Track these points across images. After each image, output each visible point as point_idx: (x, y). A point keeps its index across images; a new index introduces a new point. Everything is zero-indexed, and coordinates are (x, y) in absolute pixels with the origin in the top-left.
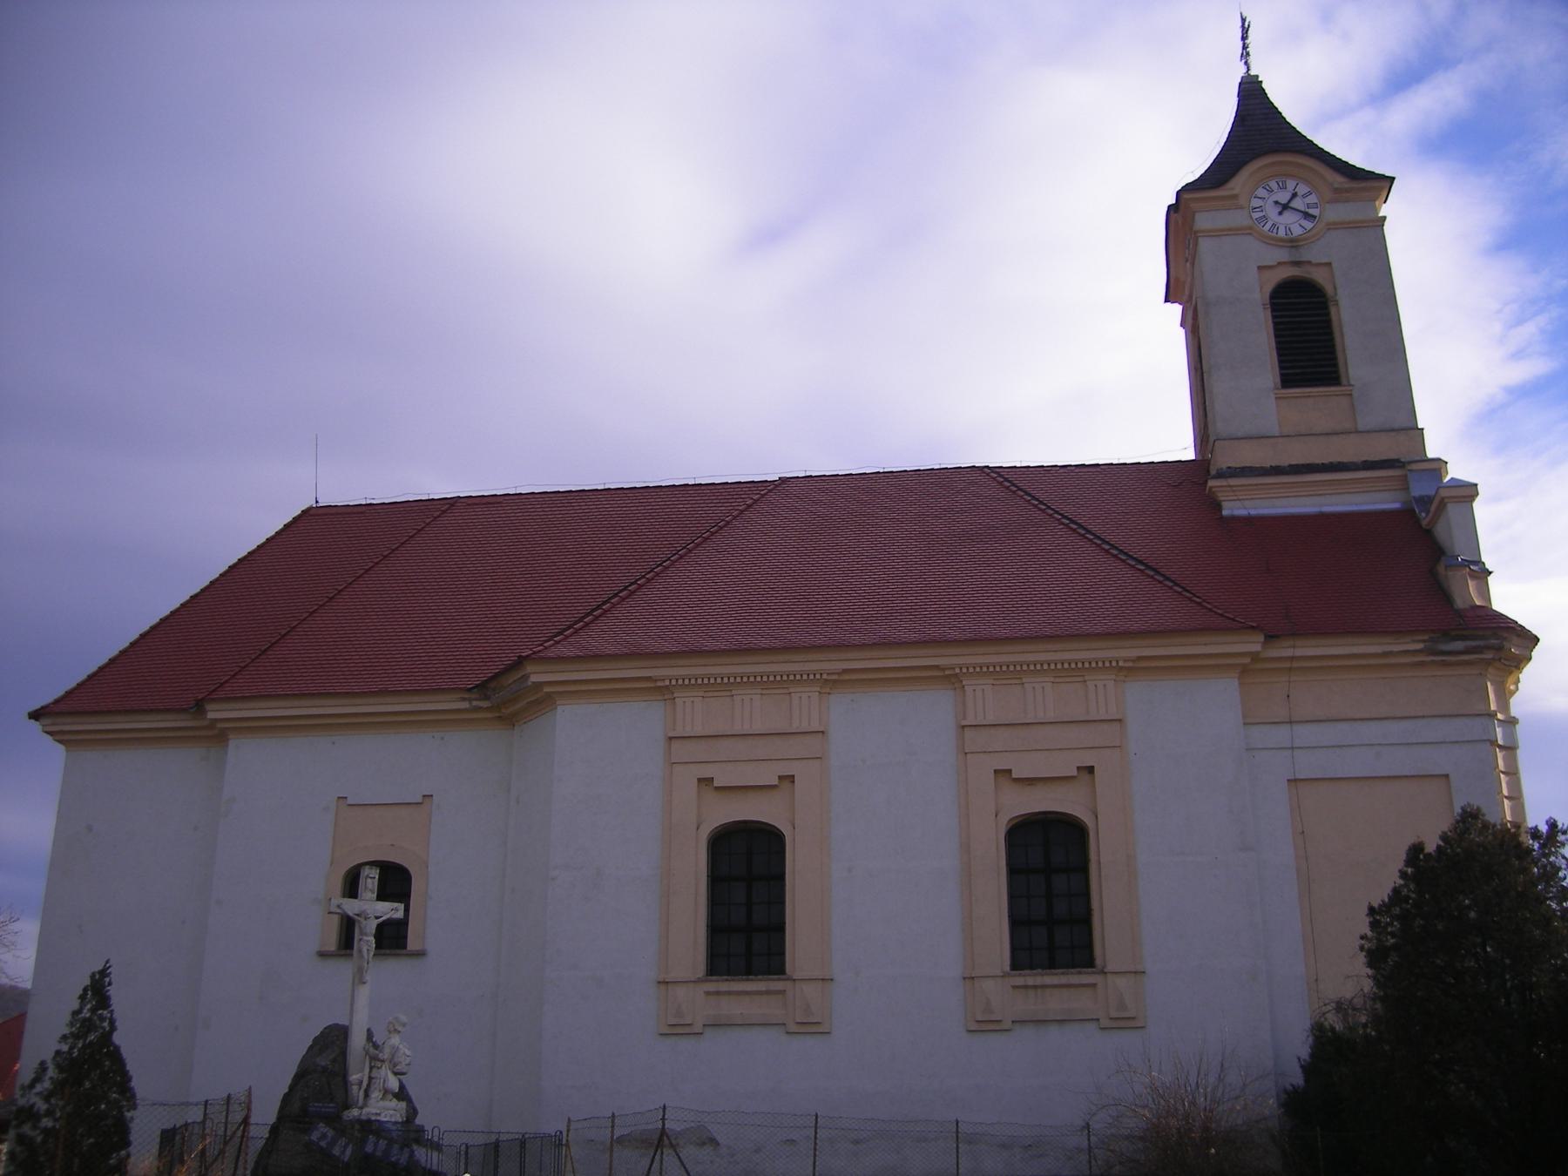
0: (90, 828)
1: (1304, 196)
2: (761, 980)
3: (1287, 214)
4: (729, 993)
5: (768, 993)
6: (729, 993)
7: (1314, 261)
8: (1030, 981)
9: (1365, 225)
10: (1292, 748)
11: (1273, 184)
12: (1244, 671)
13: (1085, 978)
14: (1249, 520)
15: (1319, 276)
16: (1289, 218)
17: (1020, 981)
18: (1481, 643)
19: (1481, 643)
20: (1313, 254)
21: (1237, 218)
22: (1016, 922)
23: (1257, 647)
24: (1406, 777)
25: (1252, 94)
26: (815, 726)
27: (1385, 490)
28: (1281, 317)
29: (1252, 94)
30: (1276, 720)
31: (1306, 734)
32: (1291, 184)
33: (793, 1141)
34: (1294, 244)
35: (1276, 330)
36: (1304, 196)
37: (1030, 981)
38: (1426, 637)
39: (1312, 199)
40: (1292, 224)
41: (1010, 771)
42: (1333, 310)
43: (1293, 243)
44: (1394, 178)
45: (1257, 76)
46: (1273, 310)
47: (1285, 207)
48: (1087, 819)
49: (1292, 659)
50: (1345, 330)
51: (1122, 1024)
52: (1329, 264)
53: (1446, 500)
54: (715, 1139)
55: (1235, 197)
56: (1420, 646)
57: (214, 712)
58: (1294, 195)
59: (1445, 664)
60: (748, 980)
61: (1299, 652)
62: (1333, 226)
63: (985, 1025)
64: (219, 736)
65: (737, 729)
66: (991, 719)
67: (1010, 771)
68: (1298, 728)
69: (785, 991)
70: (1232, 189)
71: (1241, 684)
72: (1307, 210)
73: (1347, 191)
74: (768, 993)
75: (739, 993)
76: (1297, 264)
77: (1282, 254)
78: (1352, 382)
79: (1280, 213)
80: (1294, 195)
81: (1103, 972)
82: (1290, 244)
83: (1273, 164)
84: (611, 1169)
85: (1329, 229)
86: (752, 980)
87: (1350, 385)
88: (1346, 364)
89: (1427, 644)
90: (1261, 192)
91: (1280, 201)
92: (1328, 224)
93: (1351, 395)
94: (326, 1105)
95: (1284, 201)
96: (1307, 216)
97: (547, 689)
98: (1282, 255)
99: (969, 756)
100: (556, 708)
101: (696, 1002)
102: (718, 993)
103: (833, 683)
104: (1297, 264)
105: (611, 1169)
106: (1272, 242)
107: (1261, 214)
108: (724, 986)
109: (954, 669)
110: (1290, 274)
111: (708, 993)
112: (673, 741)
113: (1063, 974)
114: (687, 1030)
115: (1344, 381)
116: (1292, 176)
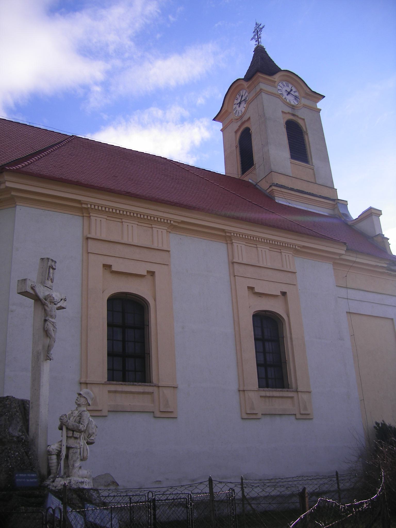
2: (140, 385)
4: (122, 392)
5: (143, 393)
6: (122, 392)
7: (299, 116)
8: (268, 394)
9: (313, 109)
12: (334, 264)
15: (300, 122)
23: (343, 252)
24: (381, 317)
26: (165, 248)
27: (328, 209)
30: (342, 286)
31: (352, 294)
33: (160, 481)
34: (293, 108)
37: (268, 394)
38: (388, 262)
43: (293, 107)
44: (325, 97)
47: (289, 93)
49: (354, 262)
50: (311, 145)
53: (373, 214)
54: (116, 482)
55: (275, 82)
60: (133, 385)
61: (358, 260)
65: (125, 240)
66: (245, 261)
68: (349, 291)
69: (153, 392)
70: (275, 79)
74: (143, 393)
75: (127, 392)
76: (294, 115)
79: (287, 95)
81: (297, 391)
82: (291, 107)
85: (303, 107)
86: (136, 385)
89: (388, 265)
90: (280, 84)
91: (287, 90)
92: (303, 105)
94: (29, 475)
97: (13, 193)
100: (16, 207)
102: (115, 392)
104: (294, 115)
106: (286, 104)
108: (120, 388)
109: (231, 233)
110: (292, 118)
111: (110, 392)
112: (90, 254)
113: (281, 391)
115: (311, 163)
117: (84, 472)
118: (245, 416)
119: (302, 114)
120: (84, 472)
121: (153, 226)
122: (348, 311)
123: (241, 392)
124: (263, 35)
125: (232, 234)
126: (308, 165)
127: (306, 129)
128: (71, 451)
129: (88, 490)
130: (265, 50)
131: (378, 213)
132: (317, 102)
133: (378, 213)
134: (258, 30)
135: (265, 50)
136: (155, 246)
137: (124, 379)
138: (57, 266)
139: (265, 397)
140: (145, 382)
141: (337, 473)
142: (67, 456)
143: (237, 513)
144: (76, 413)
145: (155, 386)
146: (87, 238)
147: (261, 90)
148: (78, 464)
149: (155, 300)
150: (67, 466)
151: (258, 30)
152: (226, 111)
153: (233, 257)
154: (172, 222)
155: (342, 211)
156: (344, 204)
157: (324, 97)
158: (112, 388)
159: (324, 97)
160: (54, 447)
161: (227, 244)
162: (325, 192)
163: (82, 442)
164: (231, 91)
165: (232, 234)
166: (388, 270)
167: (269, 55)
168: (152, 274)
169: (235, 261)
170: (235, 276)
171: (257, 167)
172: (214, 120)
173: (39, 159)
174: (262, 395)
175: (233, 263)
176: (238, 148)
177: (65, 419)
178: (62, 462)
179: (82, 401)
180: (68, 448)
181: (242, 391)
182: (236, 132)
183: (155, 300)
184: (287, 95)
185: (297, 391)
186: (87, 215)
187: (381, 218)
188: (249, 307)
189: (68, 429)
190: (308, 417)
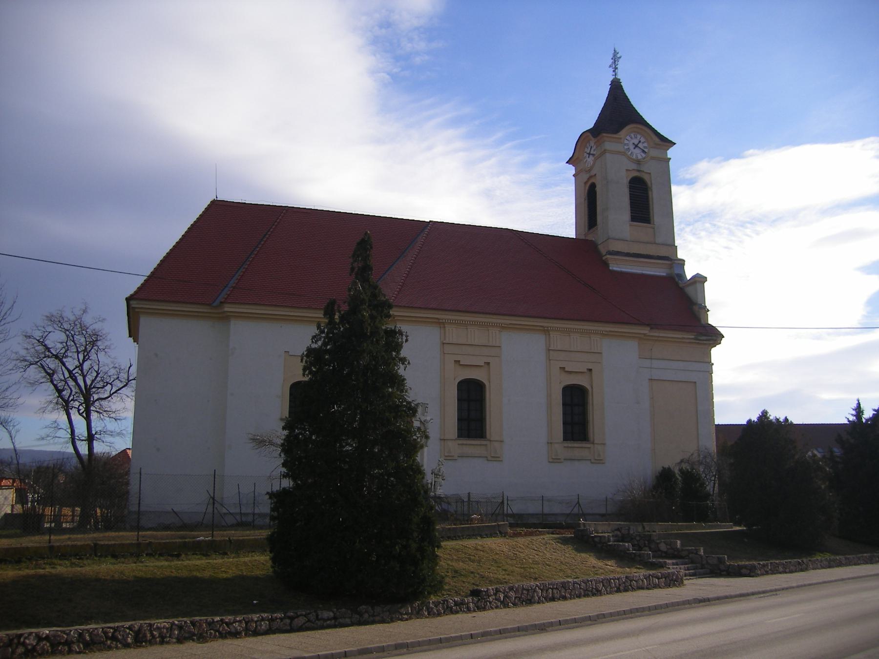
0: (156, 355)
1: (643, 143)
3: (637, 148)
4: (466, 444)
5: (481, 445)
6: (466, 444)
7: (645, 171)
10: (651, 368)
11: (633, 136)
13: (584, 445)
14: (622, 274)
15: (646, 177)
16: (637, 151)
17: (566, 445)
18: (710, 338)
19: (710, 338)
20: (645, 168)
21: (619, 147)
22: (564, 423)
25: (616, 88)
28: (632, 191)
29: (616, 88)
32: (639, 136)
35: (630, 197)
36: (643, 143)
37: (570, 445)
38: (695, 334)
39: (646, 145)
40: (637, 154)
41: (564, 368)
42: (650, 193)
43: (638, 162)
45: (620, 79)
46: (630, 188)
47: (636, 146)
48: (589, 387)
49: (659, 337)
51: (598, 462)
52: (650, 173)
55: (621, 138)
56: (693, 337)
57: (228, 308)
58: (640, 142)
59: (698, 343)
61: (661, 335)
62: (653, 158)
63: (555, 460)
64: (225, 318)
66: (559, 348)
67: (564, 368)
71: (638, 343)
72: (644, 149)
73: (659, 145)
74: (481, 445)
76: (639, 171)
77: (634, 166)
78: (655, 223)
79: (634, 148)
80: (640, 142)
81: (593, 443)
83: (634, 127)
84: (578, 499)
87: (654, 225)
88: (653, 216)
90: (628, 138)
92: (651, 157)
93: (654, 228)
95: (636, 143)
96: (643, 151)
98: (634, 167)
99: (551, 361)
101: (455, 447)
103: (503, 327)
104: (639, 171)
105: (578, 499)
107: (628, 147)
108: (465, 442)
109: (548, 328)
112: (445, 345)
114: (498, 459)
115: (652, 223)
116: (638, 133)
117: (441, 491)
118: (551, 460)
119: (650, 169)
120: (441, 491)
121: (489, 329)
122: (650, 378)
123: (549, 444)
124: (621, 65)
125: (549, 328)
126: (649, 225)
127: (651, 184)
128: (436, 483)
129: (444, 497)
130: (621, 84)
131: (704, 279)
132: (668, 150)
133: (704, 279)
134: (616, 58)
135: (621, 84)
136: (491, 344)
137: (469, 436)
138: (429, 406)
139: (568, 447)
140: (482, 437)
141: (469, 494)
142: (434, 485)
143: (255, 445)
144: (438, 468)
145: (488, 440)
146: (444, 343)
147: (605, 150)
148: (439, 488)
149: (490, 382)
150: (434, 488)
151: (616, 58)
152: (578, 158)
153: (550, 347)
154: (503, 325)
155: (677, 271)
156: (682, 263)
157: (675, 144)
158: (460, 442)
159: (675, 144)
160: (430, 481)
161: (546, 335)
162: (663, 252)
163: (440, 480)
164: (581, 140)
165: (549, 328)
166: (695, 340)
167: (625, 92)
168: (488, 364)
169: (550, 348)
170: (550, 360)
171: (599, 229)
172: (567, 163)
173: (408, 275)
174: (565, 446)
175: (549, 350)
176: (586, 201)
177: (434, 471)
178: (433, 487)
179: (440, 463)
180: (435, 482)
181: (550, 443)
182: (586, 183)
183: (490, 382)
184: (634, 148)
185: (593, 443)
186: (443, 326)
187: (706, 284)
188: (560, 383)
189: (435, 474)
190: (601, 462)
